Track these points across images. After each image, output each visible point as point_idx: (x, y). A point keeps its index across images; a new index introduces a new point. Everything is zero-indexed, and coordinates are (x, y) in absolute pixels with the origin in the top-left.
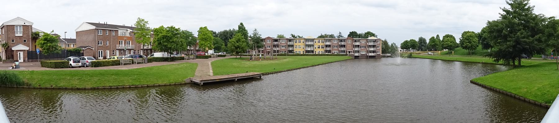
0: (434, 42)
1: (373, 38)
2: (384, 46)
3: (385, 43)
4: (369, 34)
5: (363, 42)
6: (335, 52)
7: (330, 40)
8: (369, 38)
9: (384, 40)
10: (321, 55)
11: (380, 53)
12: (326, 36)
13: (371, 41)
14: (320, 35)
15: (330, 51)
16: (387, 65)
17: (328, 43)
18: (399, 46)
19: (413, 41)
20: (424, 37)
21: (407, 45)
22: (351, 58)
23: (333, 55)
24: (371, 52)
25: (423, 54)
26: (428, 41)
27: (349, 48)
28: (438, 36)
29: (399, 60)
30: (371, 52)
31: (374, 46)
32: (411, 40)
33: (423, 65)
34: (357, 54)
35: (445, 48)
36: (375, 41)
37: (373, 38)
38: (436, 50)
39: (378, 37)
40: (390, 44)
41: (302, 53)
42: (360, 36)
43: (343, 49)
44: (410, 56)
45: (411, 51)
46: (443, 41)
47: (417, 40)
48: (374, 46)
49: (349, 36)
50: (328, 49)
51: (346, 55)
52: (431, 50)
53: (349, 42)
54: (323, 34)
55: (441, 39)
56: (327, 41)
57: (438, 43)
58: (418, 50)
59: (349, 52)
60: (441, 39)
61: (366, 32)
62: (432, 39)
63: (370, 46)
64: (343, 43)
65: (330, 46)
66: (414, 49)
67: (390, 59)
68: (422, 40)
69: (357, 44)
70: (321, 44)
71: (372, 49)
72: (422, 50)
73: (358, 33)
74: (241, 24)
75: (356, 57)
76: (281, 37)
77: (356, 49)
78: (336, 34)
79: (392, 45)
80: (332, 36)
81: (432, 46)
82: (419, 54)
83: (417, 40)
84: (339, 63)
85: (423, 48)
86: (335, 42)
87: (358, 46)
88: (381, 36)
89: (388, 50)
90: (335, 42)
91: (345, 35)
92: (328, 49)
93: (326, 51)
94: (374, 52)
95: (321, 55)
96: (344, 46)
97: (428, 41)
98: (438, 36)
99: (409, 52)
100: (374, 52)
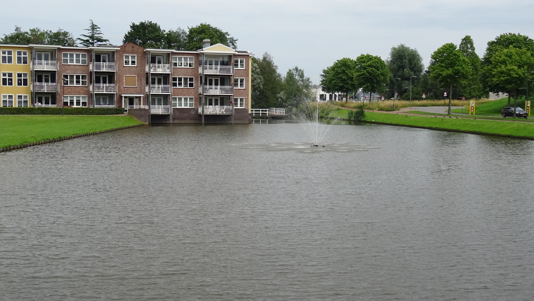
0: (452, 65)
1: (219, 49)
2: (260, 80)
3: (265, 68)
4: (205, 34)
5: (184, 62)
6: (75, 98)
7: (52, 55)
8: (208, 49)
9: (259, 56)
10: (19, 111)
11: (246, 103)
12: (36, 37)
13: (214, 59)
14: (11, 31)
15: (52, 97)
16: (274, 150)
17: (45, 66)
18: (315, 78)
19: (368, 63)
20: (411, 45)
21: (344, 78)
22: (136, 122)
23: (66, 110)
24: (211, 100)
25: (407, 109)
26: (426, 62)
27: (128, 85)
28: (467, 41)
29: (314, 131)
30: (211, 100)
31: (223, 80)
32: (363, 59)
33: (404, 155)
34: (158, 110)
35: (496, 89)
36: (227, 61)
37: (219, 49)
38: (457, 96)
39: (241, 46)
40: (282, 71)
41: (15, 105)
42: (171, 40)
43: (104, 88)
44: (358, 119)
45: (363, 98)
46: (487, 60)
47: (386, 56)
48: (223, 80)
49: (129, 39)
50: (46, 87)
51: (119, 111)
52: (438, 96)
53: (131, 60)
54: (25, 29)
55: (481, 52)
56: (39, 55)
57: (469, 69)
58: (389, 96)
59: (131, 101)
60: (481, 52)
61: (196, 24)
62: (446, 56)
63: (208, 80)
64: (105, 67)
65: (51, 76)
66: (373, 90)
67: (281, 128)
68: (404, 58)
69: (162, 69)
70: (15, 68)
71: (216, 91)
72: (403, 95)
73: (167, 26)
74: (94, 27)
75: (158, 121)
77: (157, 90)
78: (78, 32)
79: (290, 75)
80: (60, 38)
81: (444, 79)
82: (392, 108)
83: (386, 56)
84: (93, 141)
85: (408, 86)
86: (75, 62)
87: (164, 79)
88: (252, 42)
89: (274, 93)
90: (75, 62)
91: (115, 36)
92: (46, 87)
93: (38, 96)
94: (222, 100)
95: (19, 111)
96: (110, 77)
97: (426, 62)
98: (467, 41)
99: (354, 103)
100: (222, 100)
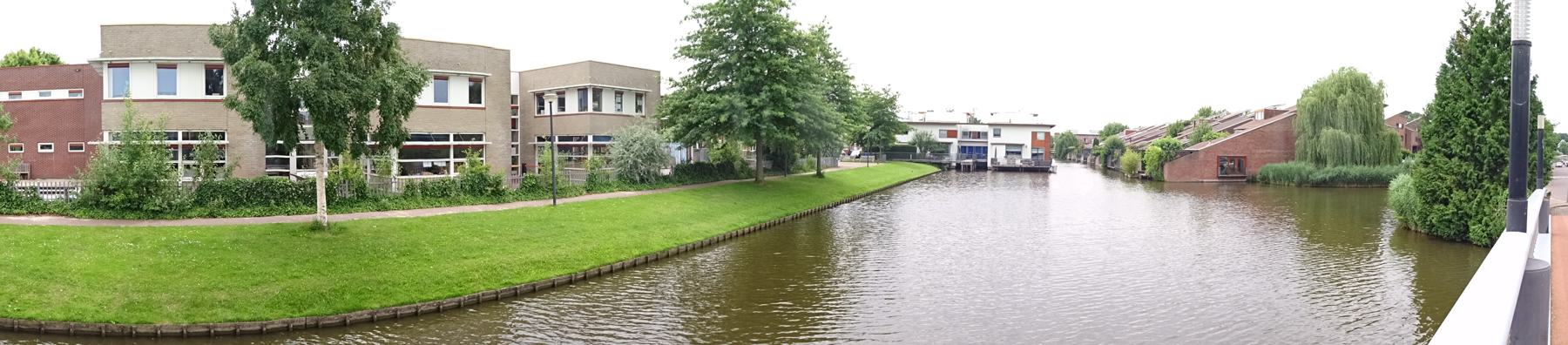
76: (1444, 67)
